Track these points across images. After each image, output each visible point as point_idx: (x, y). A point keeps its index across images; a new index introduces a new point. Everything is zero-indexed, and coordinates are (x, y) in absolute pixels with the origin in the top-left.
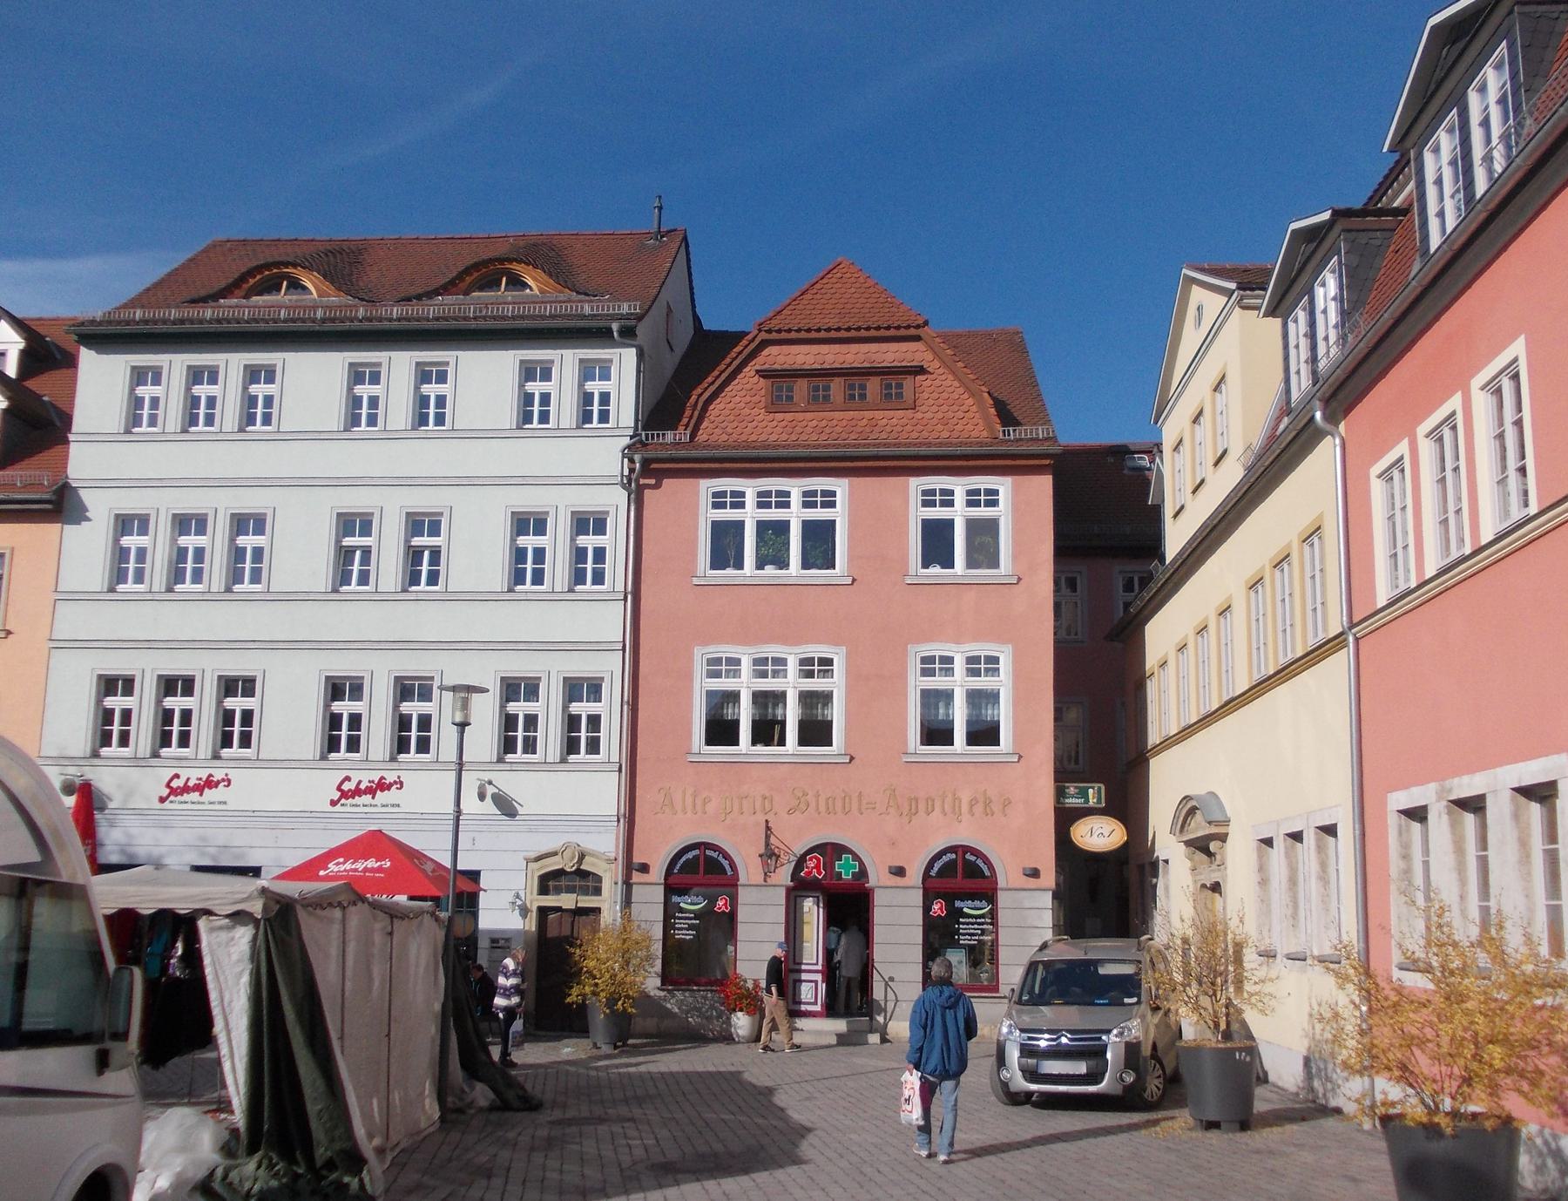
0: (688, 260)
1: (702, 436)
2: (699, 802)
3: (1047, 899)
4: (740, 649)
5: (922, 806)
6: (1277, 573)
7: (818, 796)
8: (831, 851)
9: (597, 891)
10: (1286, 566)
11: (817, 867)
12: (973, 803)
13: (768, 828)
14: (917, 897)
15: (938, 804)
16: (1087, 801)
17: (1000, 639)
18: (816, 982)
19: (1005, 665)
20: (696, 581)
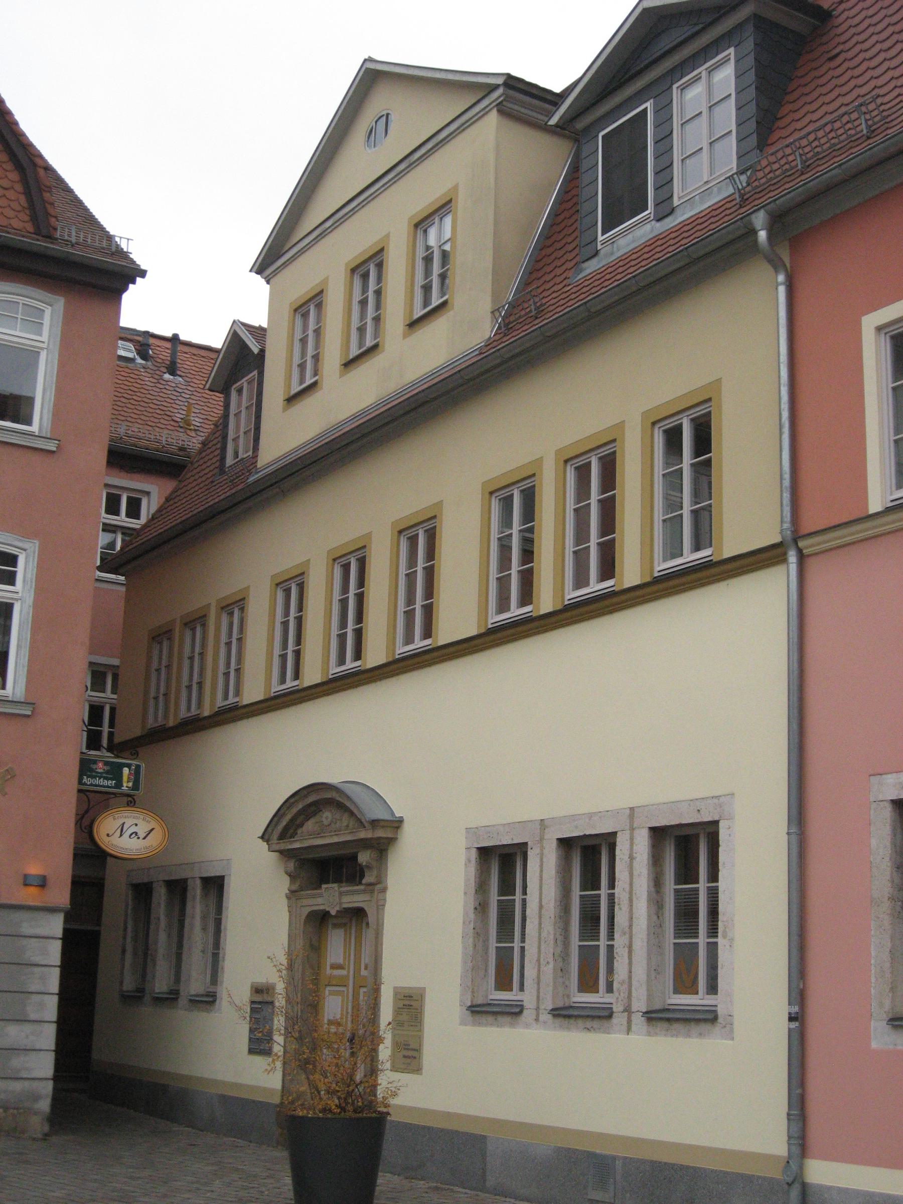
3: (56, 925)
16: (119, 785)
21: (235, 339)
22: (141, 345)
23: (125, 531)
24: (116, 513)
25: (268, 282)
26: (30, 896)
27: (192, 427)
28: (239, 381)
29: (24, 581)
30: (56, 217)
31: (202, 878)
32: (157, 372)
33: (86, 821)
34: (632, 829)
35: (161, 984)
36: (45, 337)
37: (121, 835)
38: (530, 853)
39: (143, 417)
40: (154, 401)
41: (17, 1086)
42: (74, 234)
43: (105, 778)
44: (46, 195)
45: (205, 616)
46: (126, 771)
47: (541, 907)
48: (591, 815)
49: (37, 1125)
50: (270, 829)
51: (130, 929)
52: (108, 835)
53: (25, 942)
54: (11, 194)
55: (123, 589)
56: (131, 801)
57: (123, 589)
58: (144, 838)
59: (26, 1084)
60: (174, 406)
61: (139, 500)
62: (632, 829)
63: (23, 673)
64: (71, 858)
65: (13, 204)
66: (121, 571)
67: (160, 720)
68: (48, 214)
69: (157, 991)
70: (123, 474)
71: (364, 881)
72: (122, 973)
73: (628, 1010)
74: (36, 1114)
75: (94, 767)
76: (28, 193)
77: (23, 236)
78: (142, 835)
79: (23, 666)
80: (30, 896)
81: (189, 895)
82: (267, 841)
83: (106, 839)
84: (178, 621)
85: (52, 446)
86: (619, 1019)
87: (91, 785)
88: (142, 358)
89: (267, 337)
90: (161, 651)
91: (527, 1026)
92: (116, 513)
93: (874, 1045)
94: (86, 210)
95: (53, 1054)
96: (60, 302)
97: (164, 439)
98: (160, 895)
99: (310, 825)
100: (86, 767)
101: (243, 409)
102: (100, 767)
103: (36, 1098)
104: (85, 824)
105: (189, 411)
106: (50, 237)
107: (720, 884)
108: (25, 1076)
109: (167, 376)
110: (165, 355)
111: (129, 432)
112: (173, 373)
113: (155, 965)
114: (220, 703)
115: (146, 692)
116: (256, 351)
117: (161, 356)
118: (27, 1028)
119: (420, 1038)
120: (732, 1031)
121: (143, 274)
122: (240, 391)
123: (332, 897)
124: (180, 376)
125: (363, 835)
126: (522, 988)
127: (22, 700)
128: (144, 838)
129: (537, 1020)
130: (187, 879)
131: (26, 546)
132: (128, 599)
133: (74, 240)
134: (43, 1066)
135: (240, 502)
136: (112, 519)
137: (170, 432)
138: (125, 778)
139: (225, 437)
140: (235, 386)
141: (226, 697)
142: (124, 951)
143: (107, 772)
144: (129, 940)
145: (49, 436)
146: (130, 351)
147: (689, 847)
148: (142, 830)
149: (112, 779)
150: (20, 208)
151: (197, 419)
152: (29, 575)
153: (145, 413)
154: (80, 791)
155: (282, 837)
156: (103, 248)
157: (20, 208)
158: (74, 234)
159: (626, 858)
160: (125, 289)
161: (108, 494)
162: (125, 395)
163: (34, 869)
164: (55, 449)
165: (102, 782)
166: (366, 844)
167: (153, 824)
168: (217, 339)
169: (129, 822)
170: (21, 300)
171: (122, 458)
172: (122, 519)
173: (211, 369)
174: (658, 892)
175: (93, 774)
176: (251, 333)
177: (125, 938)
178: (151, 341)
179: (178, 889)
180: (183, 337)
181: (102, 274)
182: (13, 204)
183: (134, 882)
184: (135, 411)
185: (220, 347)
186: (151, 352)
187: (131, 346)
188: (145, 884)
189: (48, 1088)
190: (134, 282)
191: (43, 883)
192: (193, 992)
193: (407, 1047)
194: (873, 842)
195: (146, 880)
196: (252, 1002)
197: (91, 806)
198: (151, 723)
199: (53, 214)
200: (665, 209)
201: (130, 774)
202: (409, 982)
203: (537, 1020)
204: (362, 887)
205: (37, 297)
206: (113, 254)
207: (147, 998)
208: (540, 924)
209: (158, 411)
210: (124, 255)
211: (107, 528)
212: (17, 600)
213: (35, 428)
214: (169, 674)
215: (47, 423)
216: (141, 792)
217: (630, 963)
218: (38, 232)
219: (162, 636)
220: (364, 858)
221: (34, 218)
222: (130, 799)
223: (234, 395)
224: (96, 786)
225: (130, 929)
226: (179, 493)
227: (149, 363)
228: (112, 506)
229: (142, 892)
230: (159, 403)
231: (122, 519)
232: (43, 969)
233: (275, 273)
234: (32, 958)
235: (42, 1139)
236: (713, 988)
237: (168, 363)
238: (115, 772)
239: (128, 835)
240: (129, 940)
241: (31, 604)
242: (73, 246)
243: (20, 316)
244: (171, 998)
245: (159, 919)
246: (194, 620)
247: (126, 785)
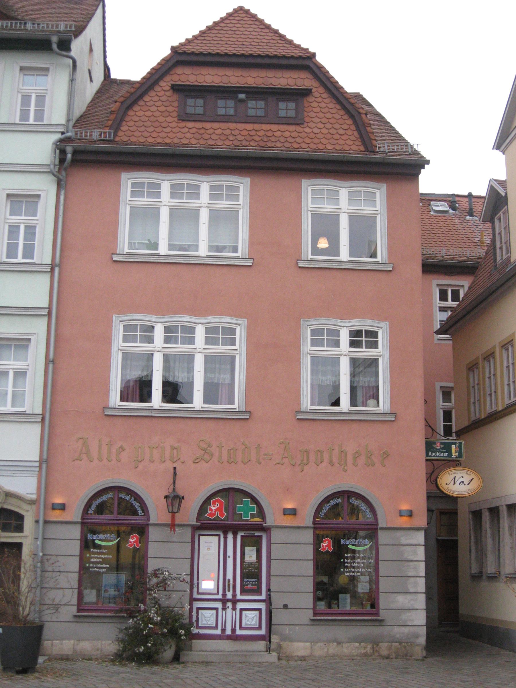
0: (104, 18)
1: (122, 136)
2: (114, 450)
3: (420, 538)
4: (152, 318)
5: (312, 457)
6: (486, 364)
7: (220, 447)
8: (230, 493)
9: (19, 528)
10: (491, 360)
11: (219, 509)
12: (356, 456)
13: (175, 474)
14: (309, 536)
15: (326, 456)
16: (450, 455)
17: (381, 319)
18: (216, 609)
19: (383, 338)
20: (116, 258)
21: (492, 190)
22: (451, 203)
23: (452, 309)
24: (446, 300)
25: (504, 153)
26: (404, 522)
27: (485, 245)
29: (383, 345)
30: (375, 140)
31: (507, 505)
32: (462, 216)
33: (433, 477)
35: (490, 569)
36: (378, 208)
37: (454, 484)
39: (455, 243)
40: (462, 233)
41: (406, 630)
42: (386, 147)
43: (442, 452)
44: (368, 129)
45: (493, 353)
46: (453, 446)
49: (419, 652)
51: (472, 537)
52: (446, 484)
53: (404, 548)
54: (349, 132)
55: (451, 342)
56: (457, 463)
57: (451, 342)
58: (468, 485)
59: (411, 629)
60: (473, 234)
61: (458, 291)
64: (426, 499)
65: (351, 137)
66: (449, 332)
67: (477, 415)
68: (371, 139)
69: (489, 573)
70: (447, 277)
72: (470, 563)
74: (417, 645)
75: (434, 446)
76: (358, 129)
77: (358, 154)
78: (466, 482)
79: (388, 393)
80: (404, 522)
81: (501, 517)
83: (446, 487)
84: (480, 357)
87: (434, 456)
88: (453, 210)
89: (507, 185)
90: (474, 376)
92: (446, 300)
94: (397, 132)
95: (425, 611)
96: (384, 187)
97: (468, 254)
98: (486, 516)
100: (429, 447)
101: (502, 230)
102: (438, 446)
103: (417, 636)
104: (432, 479)
105: (482, 235)
106: (374, 152)
109: (468, 218)
110: (466, 205)
111: (448, 253)
112: (471, 215)
113: (486, 557)
114: (507, 402)
115: (469, 399)
116: (503, 194)
117: (463, 207)
118: (409, 597)
121: (428, 162)
122: (500, 219)
124: (476, 216)
127: (389, 412)
128: (468, 485)
130: (498, 507)
131: (381, 325)
132: (454, 349)
133: (387, 151)
134: (420, 618)
135: (503, 284)
136: (444, 304)
137: (472, 249)
138: (453, 451)
139: (495, 247)
140: (496, 217)
141: (510, 398)
142: (470, 551)
143: (443, 448)
144: (472, 544)
145: (387, 262)
146: (445, 206)
148: (466, 480)
149: (446, 452)
150: (355, 139)
151: (487, 239)
152: (385, 342)
153: (456, 241)
154: (427, 460)
156: (404, 152)
157: (355, 139)
158: (386, 147)
160: (419, 173)
161: (440, 290)
162: (444, 232)
163: (405, 507)
164: (391, 269)
165: (440, 454)
167: (472, 476)
168: (482, 191)
169: (458, 476)
170: (362, 189)
171: (430, 268)
172: (450, 303)
173: (479, 208)
175: (435, 450)
176: (500, 184)
177: (470, 543)
178: (457, 199)
179: (494, 511)
180: (474, 194)
181: (405, 167)
182: (351, 137)
183: (473, 510)
184: (451, 240)
185: (485, 195)
186: (457, 205)
187: (445, 204)
188: (478, 511)
189: (423, 631)
190: (424, 168)
191: (410, 514)
195: (478, 509)
198: (473, 418)
199: (373, 138)
201: (456, 448)
205: (369, 186)
206: (410, 154)
207: (484, 577)
209: (464, 238)
210: (416, 153)
211: (442, 309)
212: (380, 356)
213: (379, 259)
214: (479, 389)
216: (463, 458)
218: (367, 150)
219: (472, 367)
221: (364, 142)
222: (457, 462)
223: (497, 222)
224: (436, 456)
225: (472, 537)
226: (475, 283)
227: (457, 212)
228: (443, 296)
229: (477, 515)
230: (465, 234)
231: (450, 303)
232: (416, 563)
233: (507, 147)
234: (409, 557)
235: (421, 660)
237: (468, 210)
238: (447, 447)
239: (459, 483)
240: (472, 544)
241: (388, 357)
242: (386, 154)
243: (362, 199)
244: (494, 578)
245: (486, 530)
246: (489, 356)
247: (455, 455)
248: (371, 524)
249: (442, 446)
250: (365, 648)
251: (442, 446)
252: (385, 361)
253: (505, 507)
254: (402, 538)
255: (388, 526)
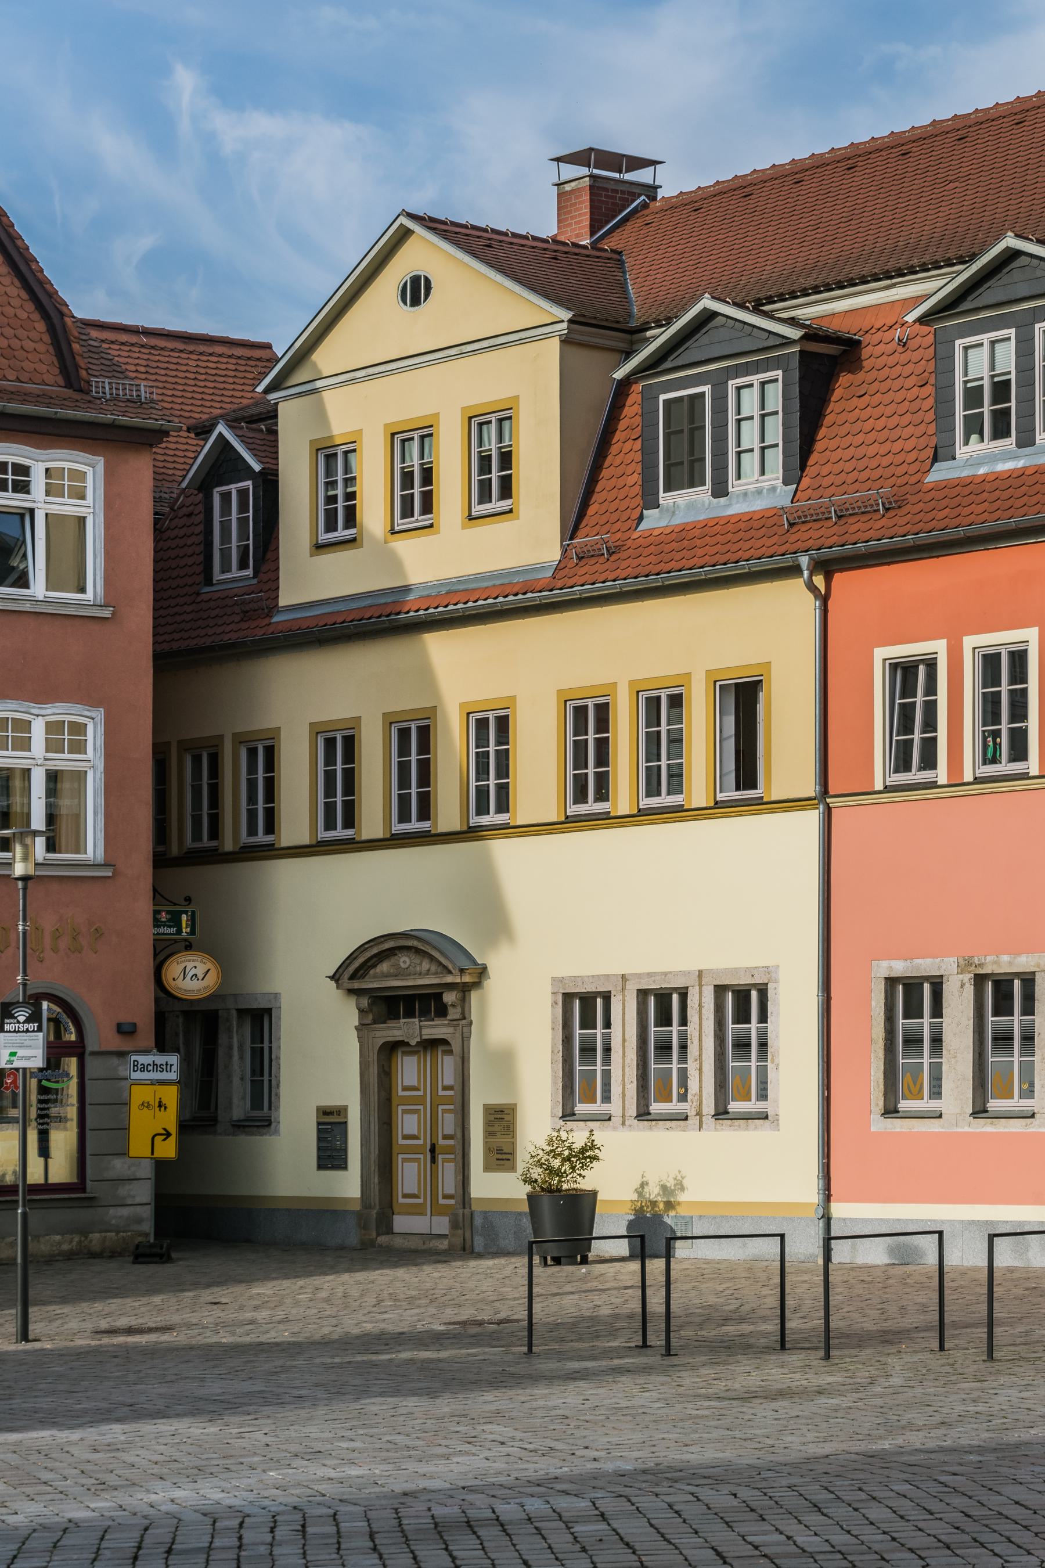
12: (57, 936)
16: (179, 931)
17: (94, 704)
28: (227, 484)
29: (95, 749)
34: (700, 986)
38: (613, 999)
41: (125, 1212)
46: (184, 917)
47: (624, 1040)
48: (665, 974)
50: (341, 971)
56: (189, 947)
59: (132, 1208)
62: (700, 986)
63: (101, 836)
71: (449, 1017)
73: (699, 1114)
78: (200, 976)
82: (337, 981)
83: (173, 983)
85: (107, 613)
86: (693, 1121)
91: (615, 1129)
93: (873, 1129)
96: (100, 462)
99: (384, 967)
103: (139, 1221)
107: (769, 1025)
108: (130, 1203)
119: (513, 1144)
120: (778, 1125)
123: (409, 1029)
125: (449, 979)
126: (607, 1098)
129: (623, 1124)
131: (93, 714)
138: (184, 925)
143: (169, 920)
147: (745, 1002)
152: (98, 743)
155: (352, 977)
159: (696, 1006)
166: (451, 986)
167: (209, 965)
174: (720, 1030)
192: (235, 1118)
193: (500, 1151)
194: (873, 1003)
196: (319, 1124)
197: (163, 952)
200: (720, 490)
201: (187, 920)
202: (497, 1099)
203: (623, 1124)
204: (446, 1022)
208: (624, 1054)
215: (100, 590)
217: (700, 1081)
220: (449, 997)
221: (64, 370)
236: (763, 1095)
247: (185, 930)
248: (271, 1061)
249: (169, 917)
250: (71, 1242)
251: (169, 917)
252: (98, 775)
253: (234, 1013)
254: (120, 1068)
255: (103, 1049)
